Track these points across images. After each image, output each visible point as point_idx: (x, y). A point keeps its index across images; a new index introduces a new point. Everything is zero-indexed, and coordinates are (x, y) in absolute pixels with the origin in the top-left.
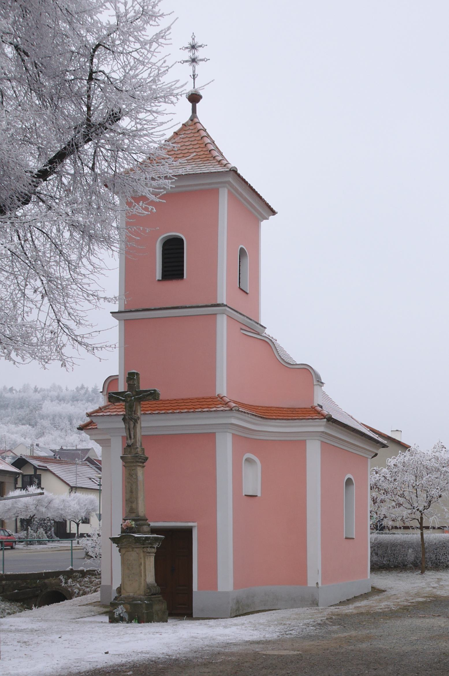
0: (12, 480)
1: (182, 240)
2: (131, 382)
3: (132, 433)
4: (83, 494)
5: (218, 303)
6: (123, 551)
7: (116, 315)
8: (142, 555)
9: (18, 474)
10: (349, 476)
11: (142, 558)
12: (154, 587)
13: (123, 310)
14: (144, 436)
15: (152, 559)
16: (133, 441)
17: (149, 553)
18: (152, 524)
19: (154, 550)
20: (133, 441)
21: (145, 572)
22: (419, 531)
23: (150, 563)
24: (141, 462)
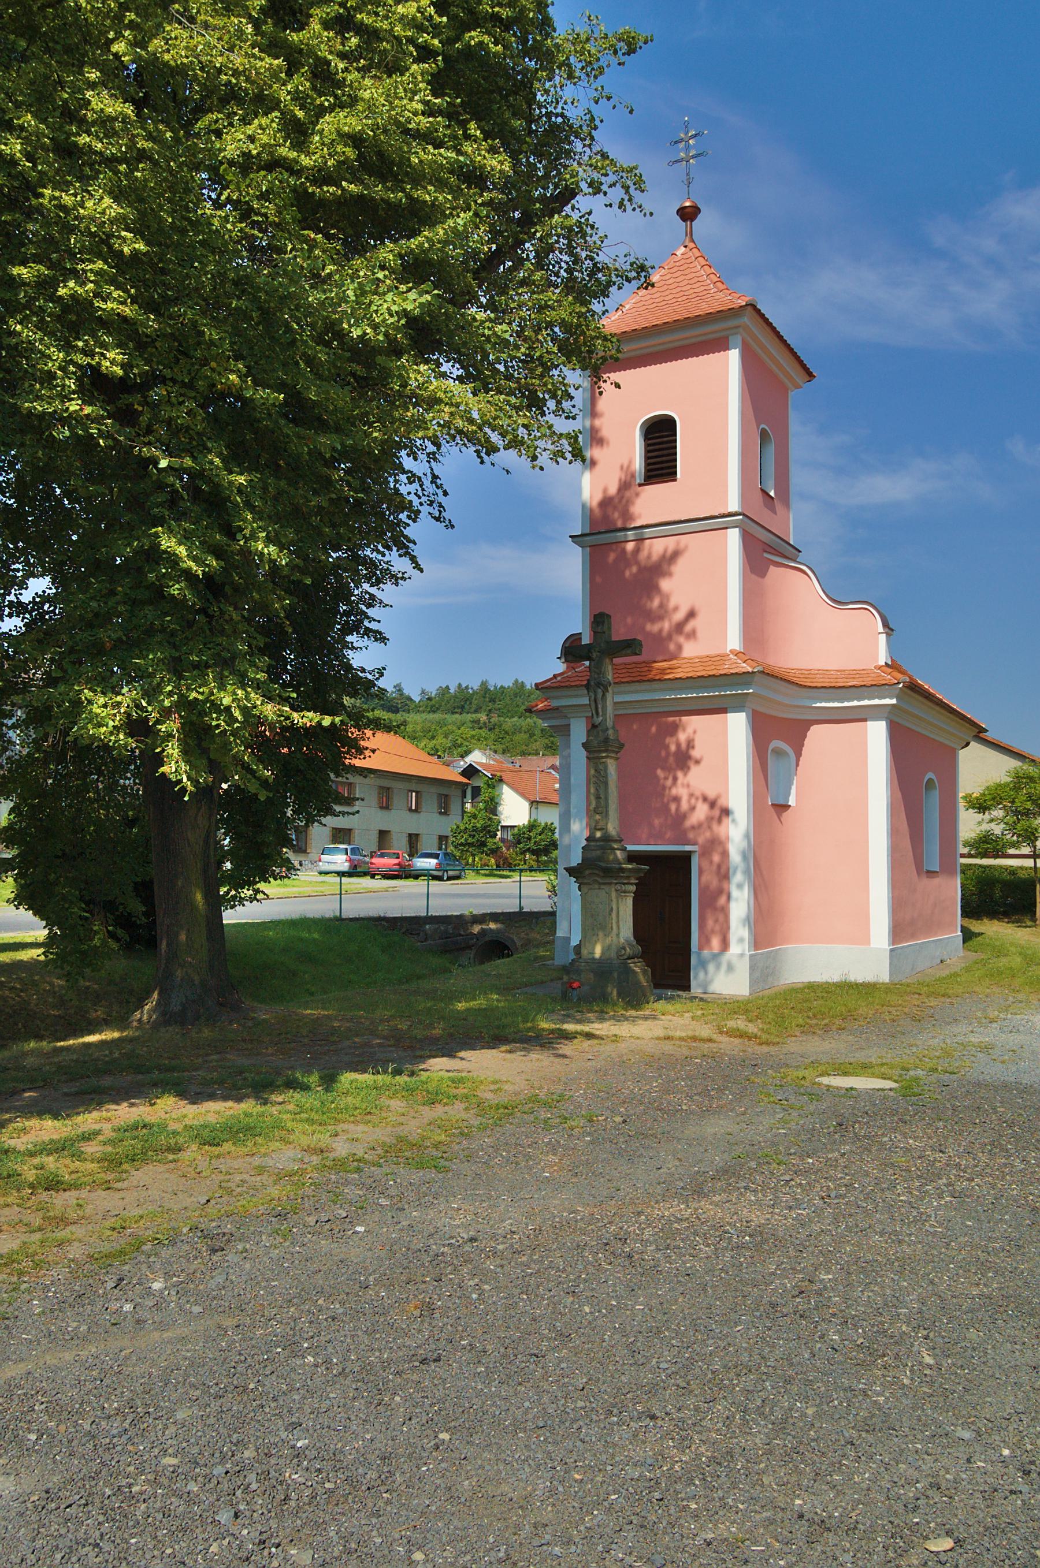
0: (459, 793)
1: (674, 422)
2: (599, 629)
3: (600, 706)
4: (747, 836)
5: (730, 510)
6: (585, 889)
7: (576, 539)
8: (614, 894)
9: (467, 784)
10: (930, 775)
11: (614, 900)
12: (630, 945)
13: (588, 531)
14: (615, 703)
15: (630, 902)
16: (601, 718)
17: (625, 892)
18: (630, 848)
19: (633, 888)
20: (601, 718)
21: (618, 922)
22: (1032, 860)
23: (626, 908)
24: (613, 752)
